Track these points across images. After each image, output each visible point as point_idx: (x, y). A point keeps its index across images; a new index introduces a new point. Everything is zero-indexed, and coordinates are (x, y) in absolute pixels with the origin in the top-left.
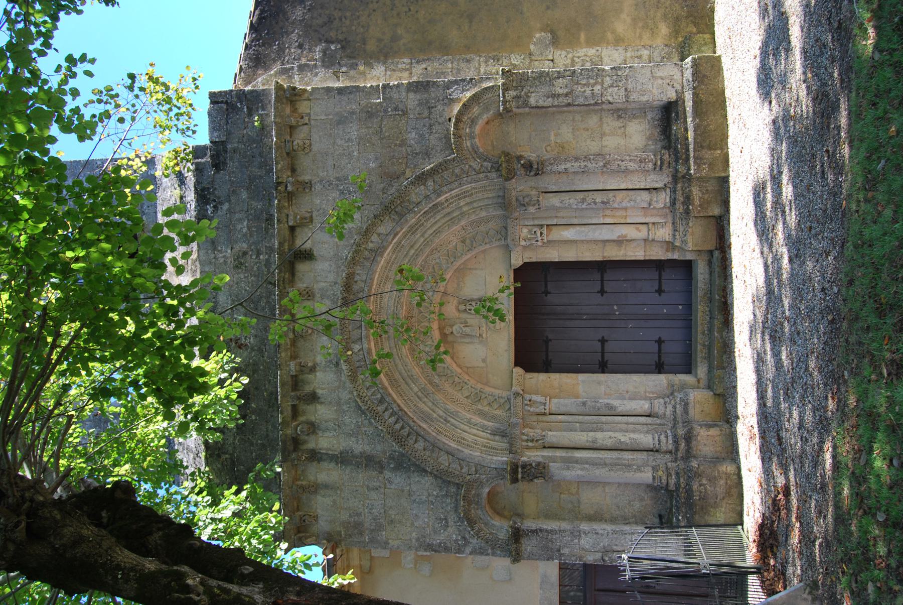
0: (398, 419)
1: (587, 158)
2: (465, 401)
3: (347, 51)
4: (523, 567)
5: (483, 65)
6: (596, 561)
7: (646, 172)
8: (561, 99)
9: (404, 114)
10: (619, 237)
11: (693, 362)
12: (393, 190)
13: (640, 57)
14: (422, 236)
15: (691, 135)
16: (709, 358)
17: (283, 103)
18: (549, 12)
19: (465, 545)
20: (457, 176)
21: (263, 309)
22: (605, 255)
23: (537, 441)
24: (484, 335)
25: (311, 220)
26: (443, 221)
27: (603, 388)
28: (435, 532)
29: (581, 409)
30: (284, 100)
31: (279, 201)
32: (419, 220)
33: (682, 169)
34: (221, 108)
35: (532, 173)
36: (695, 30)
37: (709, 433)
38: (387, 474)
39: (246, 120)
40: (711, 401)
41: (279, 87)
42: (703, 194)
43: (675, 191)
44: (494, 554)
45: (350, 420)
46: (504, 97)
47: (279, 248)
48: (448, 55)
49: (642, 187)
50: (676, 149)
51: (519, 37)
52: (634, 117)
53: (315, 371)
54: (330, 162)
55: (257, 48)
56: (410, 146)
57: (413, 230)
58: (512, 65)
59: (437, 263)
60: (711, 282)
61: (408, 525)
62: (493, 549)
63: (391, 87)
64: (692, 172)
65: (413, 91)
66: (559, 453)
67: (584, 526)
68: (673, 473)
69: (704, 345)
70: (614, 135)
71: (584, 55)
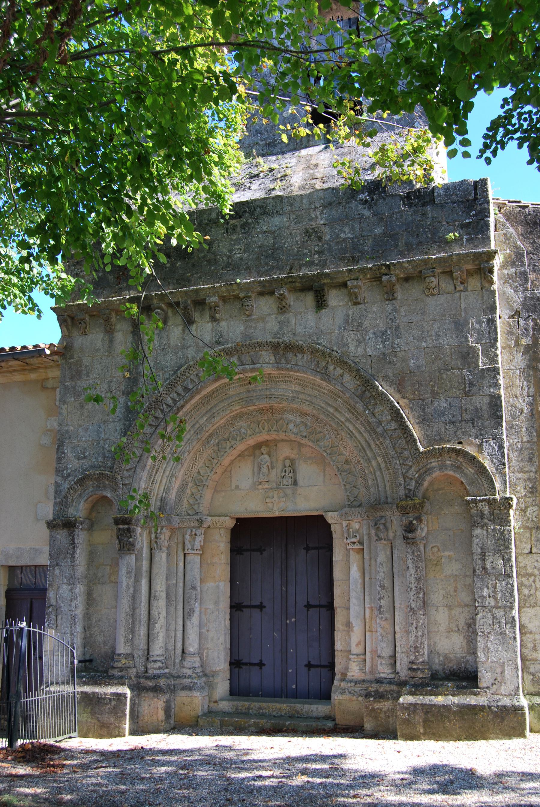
0: (170, 406)
2: (195, 470)
4: (46, 532)
6: (49, 599)
8: (480, 562)
11: (241, 698)
14: (347, 420)
16: (237, 713)
17: (474, 261)
19: (63, 477)
20: (401, 453)
21: (267, 264)
23: (156, 542)
24: (260, 487)
25: (356, 304)
27: (211, 606)
28: (73, 448)
29: (188, 584)
30: (477, 262)
34: (470, 193)
37: (160, 710)
38: (122, 400)
39: (457, 223)
40: (193, 713)
41: (491, 255)
42: (385, 712)
43: (390, 683)
44: (55, 503)
45: (169, 360)
49: (397, 649)
50: (428, 685)
53: (212, 321)
54: (415, 318)
56: (432, 402)
61: (80, 422)
62: (60, 503)
65: (491, 401)
66: (145, 565)
67: (80, 589)
68: (123, 673)
69: (249, 709)
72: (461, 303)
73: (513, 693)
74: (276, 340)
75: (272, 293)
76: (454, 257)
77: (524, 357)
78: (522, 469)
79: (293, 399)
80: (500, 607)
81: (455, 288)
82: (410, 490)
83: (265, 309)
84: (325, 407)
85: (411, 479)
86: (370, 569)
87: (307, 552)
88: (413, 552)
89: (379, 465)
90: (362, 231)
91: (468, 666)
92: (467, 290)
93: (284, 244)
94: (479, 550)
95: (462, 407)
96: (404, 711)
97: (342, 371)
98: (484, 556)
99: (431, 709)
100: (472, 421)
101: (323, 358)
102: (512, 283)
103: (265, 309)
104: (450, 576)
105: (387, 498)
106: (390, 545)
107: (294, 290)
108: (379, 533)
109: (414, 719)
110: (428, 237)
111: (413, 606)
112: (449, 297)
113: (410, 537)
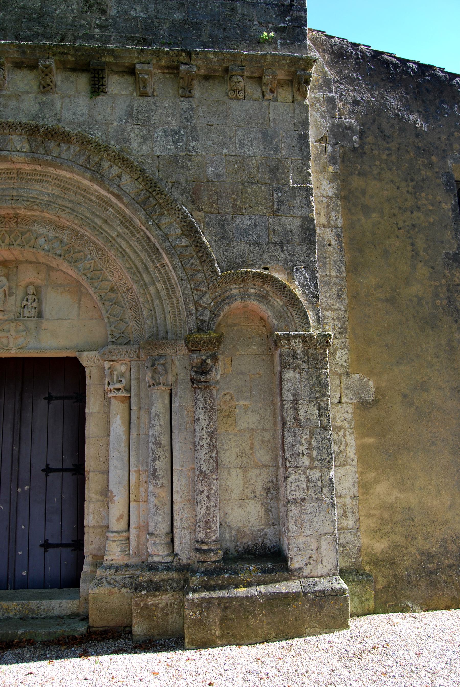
1: (212, 447)
3: (353, 153)
5: (335, 314)
7: (194, 528)
8: (291, 412)
9: (274, 212)
10: (112, 492)
12: (176, 194)
13: (344, 516)
14: (119, 235)
15: (242, 591)
17: (289, 67)
18: (400, 398)
20: (192, 276)
21: (30, 29)
22: (91, 474)
25: (143, 95)
26: (137, 262)
30: (293, 69)
31: (167, 53)
32: (139, 230)
33: (195, 580)
35: (193, 374)
36: (379, 587)
39: (270, 25)
41: (310, 62)
42: (162, 609)
43: (167, 569)
46: (295, 337)
47: (106, 49)
48: (347, 271)
49: (175, 523)
50: (223, 571)
51: (369, 360)
52: (268, 511)
54: (215, 121)
55: (355, 57)
56: (233, 218)
57: (127, 222)
58: (335, 350)
59: (85, 256)
60: (48, 619)
63: (307, 198)
64: (191, 596)
65: (303, 223)
70: (244, 483)
71: (348, 443)
72: (269, 113)
73: (331, 573)
74: (34, 122)
75: (33, 67)
76: (269, 57)
77: (331, 185)
78: (330, 306)
79: (48, 204)
80: (316, 467)
81: (264, 96)
82: (203, 321)
83: (21, 85)
84: (91, 217)
85: (205, 308)
86: (139, 423)
87: (49, 403)
88: (205, 400)
89: (158, 292)
90: (158, 12)
91: (266, 541)
92: (276, 101)
93: (56, 10)
94: (291, 397)
95: (269, 228)
96: (195, 610)
97: (120, 170)
98: (296, 404)
99: (230, 603)
100: (281, 244)
101: (94, 153)
102: (319, 107)
103: (21, 85)
104: (245, 431)
105: (167, 333)
106: (169, 391)
107: (64, 66)
108: (156, 376)
109: (208, 618)
110: (237, 34)
111: (204, 468)
112: (256, 104)
113: (202, 379)
